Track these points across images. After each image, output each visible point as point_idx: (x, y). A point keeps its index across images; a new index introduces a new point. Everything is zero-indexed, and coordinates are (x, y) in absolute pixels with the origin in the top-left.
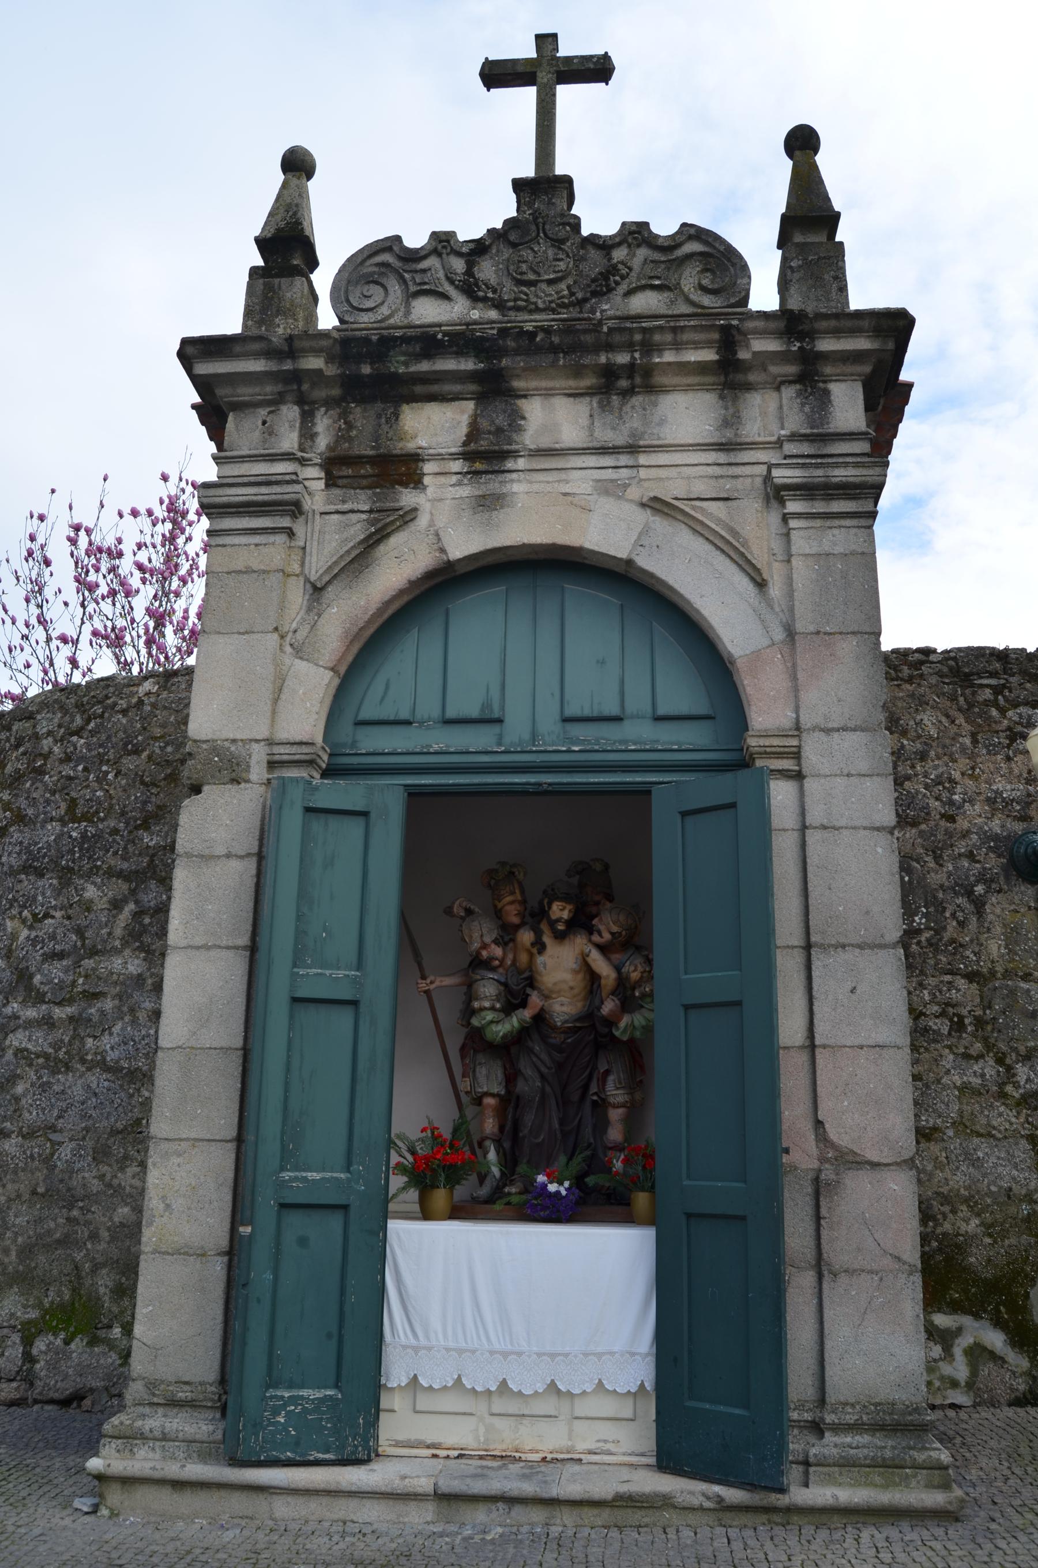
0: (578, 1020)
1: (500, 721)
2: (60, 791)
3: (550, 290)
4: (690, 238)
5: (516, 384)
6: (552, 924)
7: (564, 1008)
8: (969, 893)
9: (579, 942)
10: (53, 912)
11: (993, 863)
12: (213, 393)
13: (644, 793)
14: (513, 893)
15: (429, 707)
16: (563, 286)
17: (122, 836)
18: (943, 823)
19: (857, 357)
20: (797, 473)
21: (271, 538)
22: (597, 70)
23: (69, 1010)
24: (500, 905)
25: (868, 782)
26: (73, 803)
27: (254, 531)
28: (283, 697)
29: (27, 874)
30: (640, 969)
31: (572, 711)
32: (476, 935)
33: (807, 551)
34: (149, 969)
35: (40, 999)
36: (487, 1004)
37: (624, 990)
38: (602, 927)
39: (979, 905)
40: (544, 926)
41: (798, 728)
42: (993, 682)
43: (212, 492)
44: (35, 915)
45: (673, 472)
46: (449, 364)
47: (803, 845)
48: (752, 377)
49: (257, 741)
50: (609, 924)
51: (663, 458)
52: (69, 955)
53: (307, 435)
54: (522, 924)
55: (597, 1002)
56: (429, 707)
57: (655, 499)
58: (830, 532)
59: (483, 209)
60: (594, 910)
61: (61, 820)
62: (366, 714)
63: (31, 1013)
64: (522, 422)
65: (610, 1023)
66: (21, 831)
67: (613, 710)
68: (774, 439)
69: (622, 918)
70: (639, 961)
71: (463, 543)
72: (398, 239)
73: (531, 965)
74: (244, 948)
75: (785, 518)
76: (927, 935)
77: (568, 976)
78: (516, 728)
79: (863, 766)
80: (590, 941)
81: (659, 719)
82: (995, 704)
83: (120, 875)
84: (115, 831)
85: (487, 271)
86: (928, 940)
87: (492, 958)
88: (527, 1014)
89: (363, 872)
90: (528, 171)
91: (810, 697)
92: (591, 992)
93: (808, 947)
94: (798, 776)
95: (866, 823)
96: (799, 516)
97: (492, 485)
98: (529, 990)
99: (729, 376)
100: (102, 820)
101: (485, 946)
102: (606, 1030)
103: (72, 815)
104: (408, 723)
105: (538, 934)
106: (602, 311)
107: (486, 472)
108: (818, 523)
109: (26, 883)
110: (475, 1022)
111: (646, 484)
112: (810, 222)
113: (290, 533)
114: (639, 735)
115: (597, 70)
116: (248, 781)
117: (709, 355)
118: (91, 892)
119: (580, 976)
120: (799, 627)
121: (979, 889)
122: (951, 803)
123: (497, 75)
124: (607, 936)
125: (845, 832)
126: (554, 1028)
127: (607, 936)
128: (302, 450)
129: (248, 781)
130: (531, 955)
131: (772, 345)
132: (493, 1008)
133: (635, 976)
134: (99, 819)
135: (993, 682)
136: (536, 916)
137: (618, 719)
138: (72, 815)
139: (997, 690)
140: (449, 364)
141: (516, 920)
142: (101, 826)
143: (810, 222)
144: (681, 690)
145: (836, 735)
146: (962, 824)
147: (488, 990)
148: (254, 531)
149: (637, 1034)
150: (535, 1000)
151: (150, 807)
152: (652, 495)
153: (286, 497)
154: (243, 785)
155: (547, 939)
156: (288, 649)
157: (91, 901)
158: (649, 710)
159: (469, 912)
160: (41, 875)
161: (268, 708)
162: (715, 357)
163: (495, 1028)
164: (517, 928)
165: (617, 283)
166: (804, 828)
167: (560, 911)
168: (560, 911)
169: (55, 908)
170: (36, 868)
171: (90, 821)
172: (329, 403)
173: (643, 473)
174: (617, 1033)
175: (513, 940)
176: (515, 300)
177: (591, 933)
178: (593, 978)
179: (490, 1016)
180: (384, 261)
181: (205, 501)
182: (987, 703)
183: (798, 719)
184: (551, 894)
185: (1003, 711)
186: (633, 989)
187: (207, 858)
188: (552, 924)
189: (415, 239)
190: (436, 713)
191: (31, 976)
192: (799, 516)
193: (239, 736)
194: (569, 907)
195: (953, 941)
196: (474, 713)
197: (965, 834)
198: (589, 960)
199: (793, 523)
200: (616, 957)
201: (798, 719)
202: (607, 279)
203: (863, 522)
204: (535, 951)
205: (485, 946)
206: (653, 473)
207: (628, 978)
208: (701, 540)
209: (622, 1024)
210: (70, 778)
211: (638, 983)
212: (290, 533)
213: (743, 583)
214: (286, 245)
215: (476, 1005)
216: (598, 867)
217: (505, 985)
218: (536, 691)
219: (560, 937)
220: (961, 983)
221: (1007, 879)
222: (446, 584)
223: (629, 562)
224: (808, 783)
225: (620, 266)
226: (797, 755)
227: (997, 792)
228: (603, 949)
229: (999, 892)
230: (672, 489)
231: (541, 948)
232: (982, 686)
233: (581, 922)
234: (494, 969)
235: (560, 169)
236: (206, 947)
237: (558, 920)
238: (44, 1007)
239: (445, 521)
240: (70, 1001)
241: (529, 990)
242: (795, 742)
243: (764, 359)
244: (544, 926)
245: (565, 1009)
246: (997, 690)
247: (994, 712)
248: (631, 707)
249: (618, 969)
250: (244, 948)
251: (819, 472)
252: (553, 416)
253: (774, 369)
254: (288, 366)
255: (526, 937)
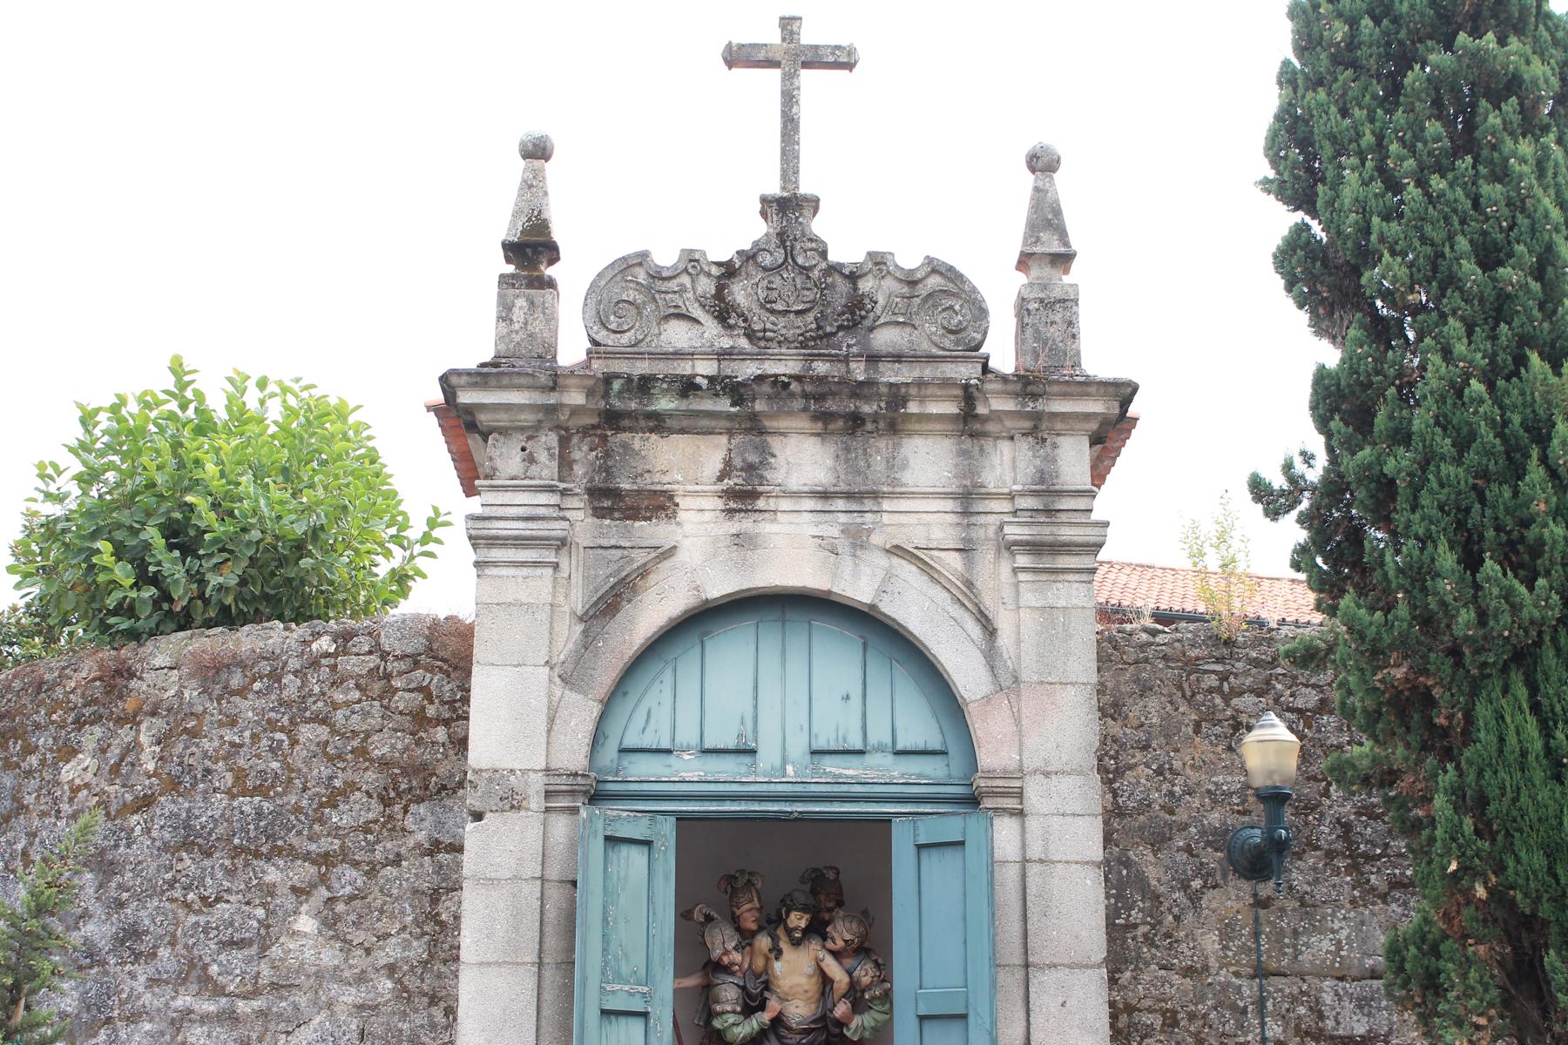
0: (813, 1022)
1: (753, 752)
2: (224, 759)
3: (799, 321)
4: (934, 271)
5: (767, 423)
6: (789, 931)
7: (799, 1011)
8: (1185, 887)
9: (814, 948)
10: (226, 896)
11: (1212, 858)
12: (454, 395)
13: (885, 822)
14: (751, 901)
15: (688, 735)
16: (810, 317)
17: (306, 815)
18: (1162, 814)
19: (1087, 417)
20: (1026, 530)
21: (539, 571)
22: (841, 60)
23: (257, 1004)
24: (738, 912)
25: (1080, 821)
26: (240, 776)
27: (523, 564)
28: (555, 728)
29: (189, 852)
30: (871, 973)
31: (821, 744)
32: (718, 941)
33: (1034, 604)
34: (346, 960)
35: (219, 991)
36: (729, 1008)
37: (855, 995)
38: (836, 935)
39: (1195, 898)
40: (781, 932)
41: (1021, 770)
42: (1219, 668)
43: (480, 524)
44: (203, 899)
45: (912, 519)
46: (708, 405)
47: (1024, 876)
48: (991, 427)
49: (535, 771)
50: (843, 932)
51: (903, 505)
52: (250, 943)
53: (565, 464)
54: (761, 929)
55: (829, 1006)
56: (688, 735)
57: (897, 547)
58: (1055, 586)
59: (736, 230)
60: (827, 916)
61: (228, 792)
62: (630, 742)
63: (210, 1007)
64: (772, 460)
65: (840, 1024)
66: (174, 802)
67: (858, 746)
68: (1006, 490)
69: (854, 925)
70: (869, 966)
71: (719, 586)
72: (644, 255)
73: (767, 969)
74: (533, 964)
75: (1015, 570)
76: (1144, 929)
77: (803, 980)
78: (768, 757)
79: (1077, 807)
80: (824, 947)
81: (898, 753)
82: (1219, 690)
83: (307, 857)
84: (297, 810)
85: (740, 294)
86: (1145, 935)
87: (733, 964)
88: (765, 1017)
89: (640, 899)
90: (774, 188)
91: (1031, 742)
92: (823, 994)
93: (1027, 966)
94: (1021, 814)
95: (1078, 858)
96: (1024, 570)
97: (744, 524)
98: (766, 994)
99: (969, 423)
100: (281, 795)
101: (726, 952)
102: (837, 1031)
103: (240, 787)
104: (669, 751)
105: (775, 939)
106: (849, 346)
107: (740, 511)
108: (1044, 577)
109: (189, 862)
110: (717, 1024)
111: (889, 529)
112: (1047, 248)
113: (556, 566)
114: (882, 770)
115: (841, 60)
116: (528, 809)
117: (951, 408)
118: (272, 875)
119: (814, 980)
120: (1024, 676)
121: (1196, 884)
122: (1171, 794)
123: (737, 57)
124: (840, 944)
125: (1059, 866)
126: (789, 1029)
127: (840, 944)
128: (561, 480)
129: (528, 809)
130: (767, 959)
131: (1009, 405)
132: (734, 1012)
133: (866, 980)
134: (277, 794)
135: (1219, 668)
136: (773, 921)
137: (861, 752)
138: (240, 787)
139: (1224, 677)
140: (708, 405)
141: (754, 927)
142: (279, 802)
143: (1047, 248)
144: (917, 724)
145: (1053, 777)
146: (1182, 816)
147: (728, 994)
148: (523, 564)
149: (867, 1034)
150: (774, 1005)
151: (337, 783)
152: (895, 542)
153: (553, 533)
154: (523, 813)
155: (784, 945)
156: (557, 680)
157: (274, 885)
158: (889, 741)
159: (709, 919)
160: (208, 854)
161: (543, 740)
162: (956, 411)
163: (736, 1030)
164: (753, 934)
165: (863, 318)
166: (1025, 861)
167: (798, 920)
168: (798, 920)
169: (228, 891)
170: (200, 846)
171: (266, 797)
172: (585, 431)
173: (886, 518)
174: (848, 1034)
175: (750, 945)
176: (765, 330)
177: (825, 939)
178: (825, 981)
179: (731, 1019)
180: (634, 286)
181: (473, 533)
182: (1210, 690)
183: (1021, 760)
184: (788, 904)
185: (1227, 699)
186: (863, 991)
187: (492, 882)
188: (789, 931)
189: (665, 257)
190: (694, 740)
191: (205, 967)
192: (1024, 570)
193: (517, 766)
194: (807, 916)
195: (1168, 935)
196: (731, 744)
197: (1184, 827)
198: (823, 965)
199: (1022, 576)
200: (849, 962)
201: (1021, 760)
202: (853, 313)
203: (1085, 577)
204: (772, 956)
205: (726, 952)
206: (896, 518)
207: (858, 982)
208: (939, 588)
209: (853, 1025)
210: (233, 745)
211: (869, 987)
212: (556, 566)
213: (975, 631)
214: (531, 251)
215: (718, 1008)
216: (831, 875)
217: (743, 988)
218: (781, 722)
219: (796, 943)
220: (1176, 979)
221: (1224, 876)
222: (703, 619)
223: (873, 607)
224: (1032, 823)
225: (867, 301)
226: (1020, 794)
227: (1216, 784)
228: (836, 955)
229: (1214, 887)
230: (914, 536)
231: (779, 953)
232: (1206, 672)
233: (818, 929)
234: (733, 974)
235: (805, 188)
236: (497, 963)
237: (796, 929)
238: (224, 1000)
239: (698, 554)
240: (256, 993)
241: (766, 994)
242: (1017, 784)
243: (997, 416)
244: (781, 932)
245: (799, 1011)
246: (1224, 677)
247: (1218, 700)
248: (873, 740)
249: (850, 973)
250: (533, 964)
251: (1047, 530)
252: (803, 459)
253: (1009, 423)
254: (552, 399)
255: (763, 942)
